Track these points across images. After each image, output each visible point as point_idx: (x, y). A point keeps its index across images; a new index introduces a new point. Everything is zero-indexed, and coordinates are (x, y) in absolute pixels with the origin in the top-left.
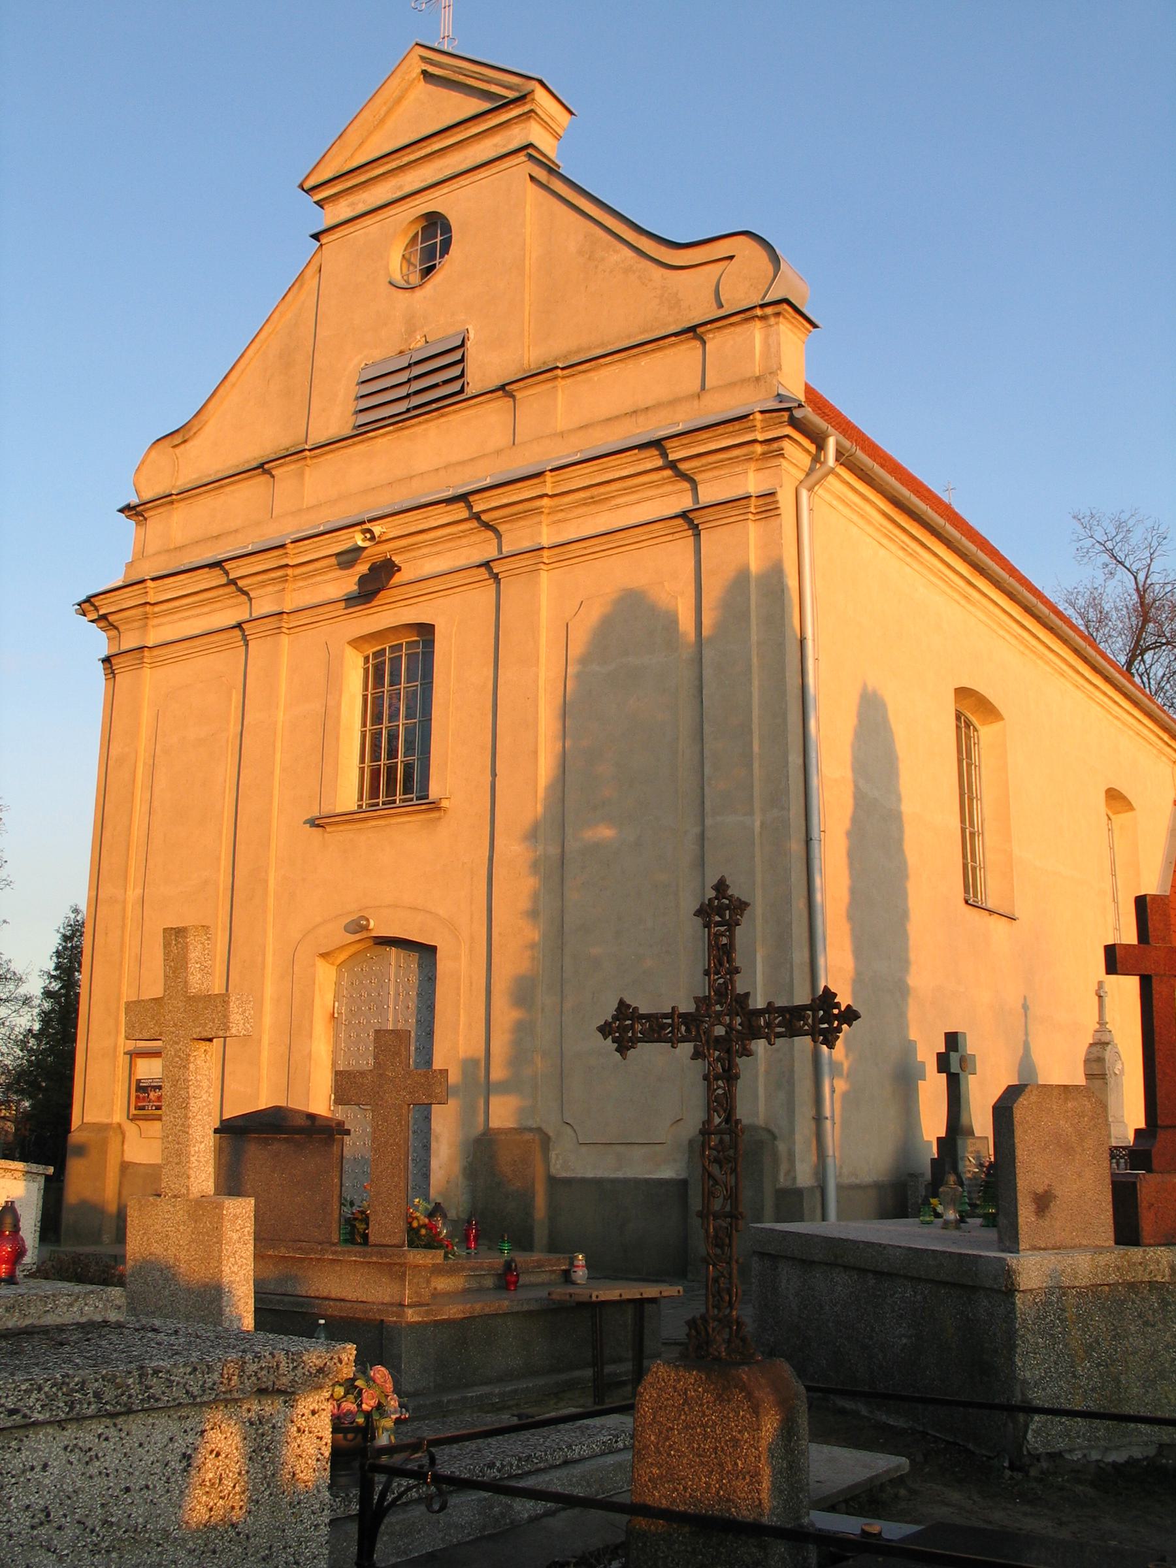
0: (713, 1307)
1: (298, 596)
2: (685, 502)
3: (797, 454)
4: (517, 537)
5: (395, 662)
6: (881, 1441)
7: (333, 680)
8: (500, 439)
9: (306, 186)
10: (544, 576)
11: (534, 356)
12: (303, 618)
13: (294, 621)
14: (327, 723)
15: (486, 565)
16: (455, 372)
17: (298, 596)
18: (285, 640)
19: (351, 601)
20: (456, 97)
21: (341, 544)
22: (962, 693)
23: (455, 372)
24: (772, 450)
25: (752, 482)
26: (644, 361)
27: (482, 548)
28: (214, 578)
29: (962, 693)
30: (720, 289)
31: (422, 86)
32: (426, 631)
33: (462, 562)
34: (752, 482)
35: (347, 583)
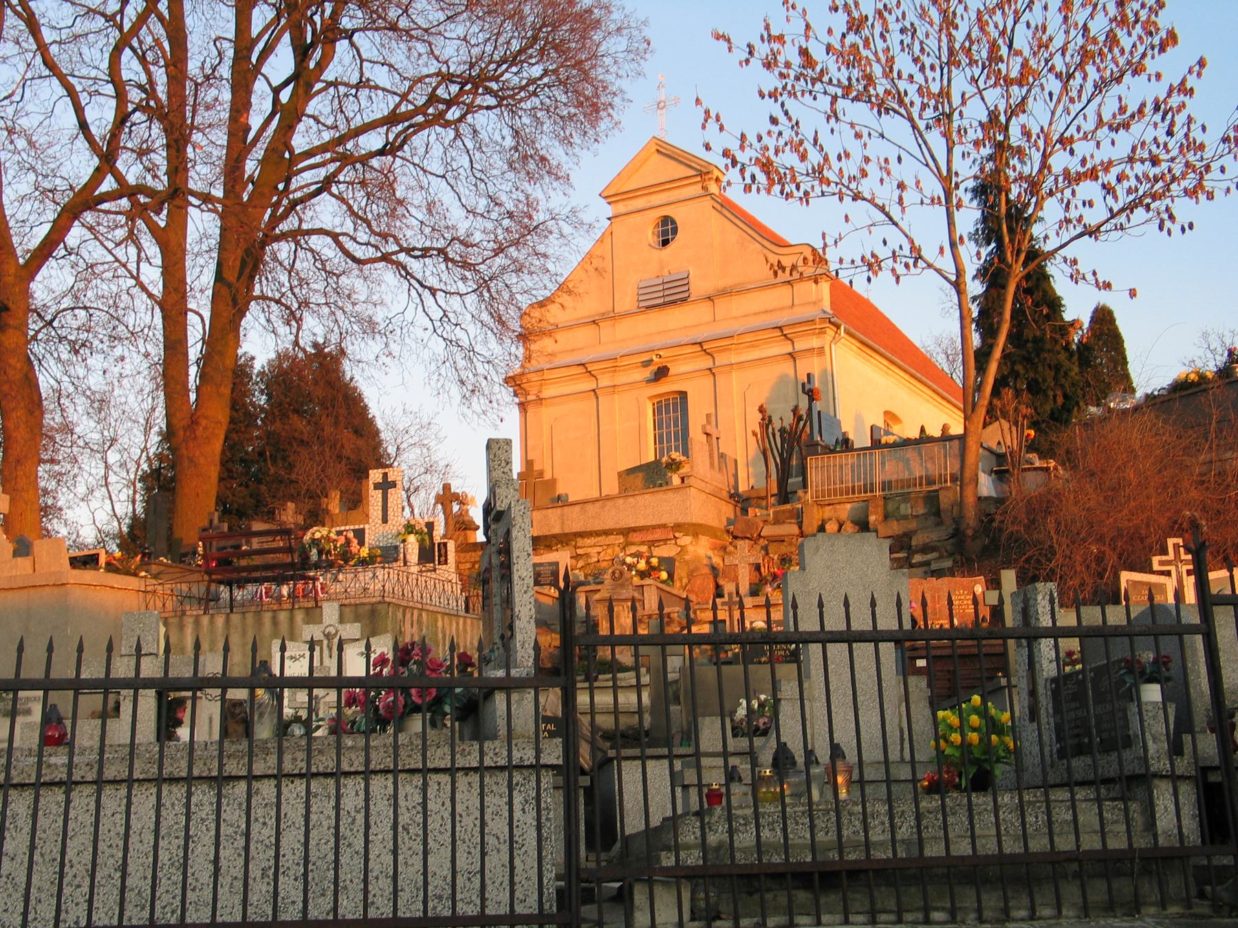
0: (724, 621)
1: (621, 378)
2: (790, 349)
3: (830, 332)
4: (721, 359)
5: (667, 406)
6: (458, 690)
7: (641, 413)
8: (709, 318)
9: (605, 194)
10: (734, 374)
11: (721, 284)
12: (626, 388)
13: (620, 389)
14: (640, 430)
15: (710, 369)
16: (686, 288)
17: (621, 378)
18: (616, 396)
19: (648, 381)
20: (682, 168)
21: (645, 358)
22: (887, 413)
23: (686, 288)
24: (822, 332)
25: (815, 342)
26: (768, 291)
27: (706, 363)
28: (582, 370)
29: (887, 413)
30: (956, 297)
31: (657, 157)
32: (683, 395)
33: (697, 367)
34: (815, 342)
35: (648, 373)
